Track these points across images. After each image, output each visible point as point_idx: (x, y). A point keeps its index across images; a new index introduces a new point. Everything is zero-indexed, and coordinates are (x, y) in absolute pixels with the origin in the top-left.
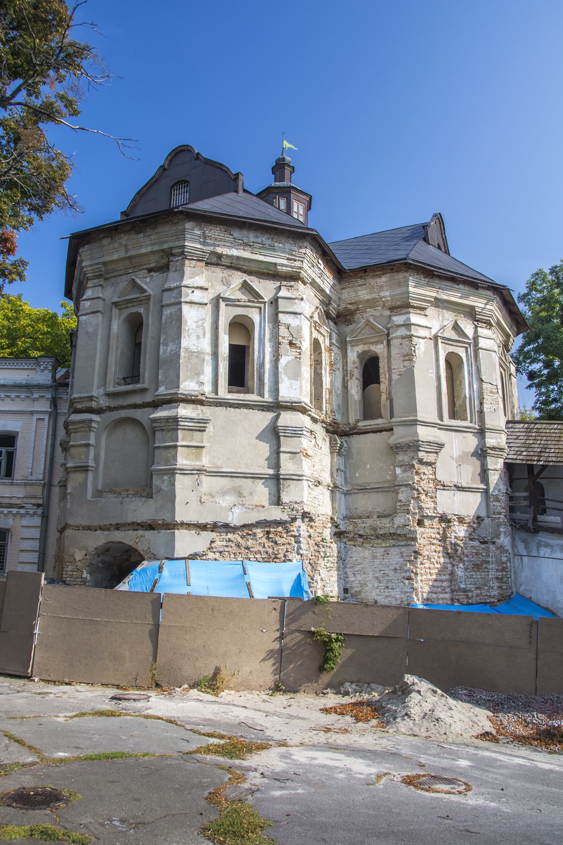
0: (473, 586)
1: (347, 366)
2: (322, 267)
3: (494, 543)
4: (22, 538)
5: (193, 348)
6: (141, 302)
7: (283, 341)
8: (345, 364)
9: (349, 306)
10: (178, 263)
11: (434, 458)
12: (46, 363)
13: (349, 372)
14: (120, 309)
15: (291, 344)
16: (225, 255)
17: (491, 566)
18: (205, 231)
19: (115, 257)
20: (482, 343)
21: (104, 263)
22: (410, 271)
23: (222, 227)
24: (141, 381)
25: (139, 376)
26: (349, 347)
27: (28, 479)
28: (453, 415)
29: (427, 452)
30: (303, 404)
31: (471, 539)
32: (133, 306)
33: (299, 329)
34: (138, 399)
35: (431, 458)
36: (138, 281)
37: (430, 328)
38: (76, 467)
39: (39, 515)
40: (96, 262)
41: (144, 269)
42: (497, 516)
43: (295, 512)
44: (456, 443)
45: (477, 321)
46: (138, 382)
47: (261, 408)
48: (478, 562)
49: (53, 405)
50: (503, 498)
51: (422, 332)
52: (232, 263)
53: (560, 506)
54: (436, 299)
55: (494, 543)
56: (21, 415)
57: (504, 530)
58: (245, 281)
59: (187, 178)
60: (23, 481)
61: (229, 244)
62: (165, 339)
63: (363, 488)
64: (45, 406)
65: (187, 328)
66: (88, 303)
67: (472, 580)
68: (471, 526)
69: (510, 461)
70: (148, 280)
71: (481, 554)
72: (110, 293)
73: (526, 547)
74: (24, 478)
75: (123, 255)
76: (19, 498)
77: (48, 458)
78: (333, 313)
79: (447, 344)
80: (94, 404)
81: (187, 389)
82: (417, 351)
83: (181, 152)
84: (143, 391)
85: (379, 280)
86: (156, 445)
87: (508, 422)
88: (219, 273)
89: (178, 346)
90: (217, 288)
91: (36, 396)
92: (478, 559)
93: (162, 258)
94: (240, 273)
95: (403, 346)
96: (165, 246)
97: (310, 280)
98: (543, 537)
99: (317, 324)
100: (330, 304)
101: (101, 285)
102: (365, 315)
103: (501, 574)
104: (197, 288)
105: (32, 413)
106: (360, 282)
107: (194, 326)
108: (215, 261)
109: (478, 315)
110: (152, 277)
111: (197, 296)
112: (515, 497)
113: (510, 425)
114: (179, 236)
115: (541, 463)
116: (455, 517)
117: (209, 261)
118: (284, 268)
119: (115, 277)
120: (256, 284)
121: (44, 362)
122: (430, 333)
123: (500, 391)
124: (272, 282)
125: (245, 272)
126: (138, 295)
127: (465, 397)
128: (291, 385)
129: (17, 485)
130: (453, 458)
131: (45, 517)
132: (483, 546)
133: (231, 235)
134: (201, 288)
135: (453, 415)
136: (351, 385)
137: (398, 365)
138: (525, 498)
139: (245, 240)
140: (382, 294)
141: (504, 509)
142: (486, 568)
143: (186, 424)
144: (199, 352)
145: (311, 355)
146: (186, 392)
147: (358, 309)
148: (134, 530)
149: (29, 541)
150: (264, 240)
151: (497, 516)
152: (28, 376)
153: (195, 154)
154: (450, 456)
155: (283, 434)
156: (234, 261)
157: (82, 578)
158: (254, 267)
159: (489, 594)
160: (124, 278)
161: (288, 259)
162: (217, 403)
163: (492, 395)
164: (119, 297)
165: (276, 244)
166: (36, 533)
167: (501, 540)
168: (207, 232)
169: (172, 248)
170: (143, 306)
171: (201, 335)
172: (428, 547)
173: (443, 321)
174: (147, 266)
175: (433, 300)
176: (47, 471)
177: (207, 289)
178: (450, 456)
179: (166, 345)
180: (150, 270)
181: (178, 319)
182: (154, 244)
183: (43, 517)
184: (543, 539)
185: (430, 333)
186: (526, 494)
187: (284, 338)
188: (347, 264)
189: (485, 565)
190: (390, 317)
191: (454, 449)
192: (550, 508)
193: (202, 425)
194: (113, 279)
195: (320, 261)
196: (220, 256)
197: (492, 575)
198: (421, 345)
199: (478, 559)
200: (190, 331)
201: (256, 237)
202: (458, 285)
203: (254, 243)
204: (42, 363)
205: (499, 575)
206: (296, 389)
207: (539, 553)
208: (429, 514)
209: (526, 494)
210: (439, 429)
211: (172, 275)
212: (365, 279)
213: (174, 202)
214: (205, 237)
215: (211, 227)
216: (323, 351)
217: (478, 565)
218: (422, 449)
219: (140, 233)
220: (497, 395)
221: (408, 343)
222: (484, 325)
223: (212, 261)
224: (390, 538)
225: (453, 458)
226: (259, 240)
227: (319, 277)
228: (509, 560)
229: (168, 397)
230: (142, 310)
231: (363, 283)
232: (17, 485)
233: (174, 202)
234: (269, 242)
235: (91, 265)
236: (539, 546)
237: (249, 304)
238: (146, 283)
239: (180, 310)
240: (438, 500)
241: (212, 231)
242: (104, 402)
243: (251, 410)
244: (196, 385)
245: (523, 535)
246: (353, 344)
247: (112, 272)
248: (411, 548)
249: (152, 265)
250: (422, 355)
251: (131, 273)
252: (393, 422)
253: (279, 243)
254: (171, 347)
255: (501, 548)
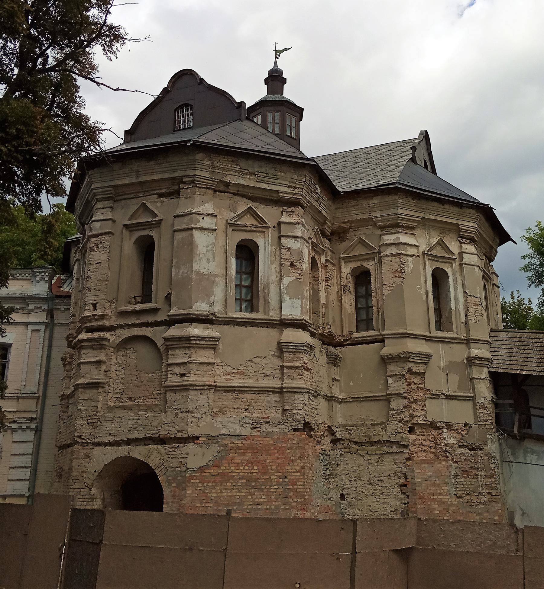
0: (463, 492)
1: (341, 281)
2: (319, 192)
3: (481, 449)
4: (12, 455)
5: (204, 271)
6: (153, 226)
7: (285, 263)
8: (339, 279)
9: (343, 225)
10: (189, 191)
11: (423, 368)
12: (43, 274)
13: (342, 287)
14: (131, 231)
15: (292, 265)
16: (232, 183)
17: (480, 473)
18: (214, 162)
19: (126, 181)
20: (467, 258)
21: (115, 187)
22: (399, 194)
23: (229, 157)
24: (153, 300)
25: (152, 295)
26: (343, 263)
27: (22, 392)
28: (439, 328)
29: (416, 363)
30: (303, 321)
31: (460, 446)
32: (144, 229)
33: (300, 253)
34: (151, 319)
35: (420, 369)
36: (148, 205)
37: (418, 246)
38: (87, 384)
39: (32, 430)
40: (106, 184)
41: (155, 194)
42: (484, 423)
43: (297, 423)
44: (442, 354)
45: (461, 237)
46: (150, 301)
47: (265, 325)
48: (468, 469)
49: (49, 316)
50: (490, 406)
51: (411, 251)
52: (238, 191)
53: (542, 413)
54: (423, 218)
55: (481, 449)
56: (15, 326)
57: (491, 436)
58: (250, 207)
59: (191, 103)
60: (16, 395)
61: (236, 174)
62: (177, 263)
63: (357, 396)
64: (42, 317)
65: (198, 252)
66: (98, 224)
67: (462, 486)
68: (459, 433)
69: (495, 370)
70: (159, 204)
71: (469, 460)
72: (123, 215)
73: (513, 454)
74: (16, 391)
75: (134, 180)
76: (11, 412)
77: (43, 370)
78: (328, 232)
79: (433, 260)
80: (107, 323)
81: (198, 309)
82: (406, 268)
83: (185, 78)
84: (155, 311)
85: (371, 202)
86: (170, 362)
87: (492, 330)
88: (226, 200)
89: (190, 269)
90: (225, 214)
91: (31, 307)
92: (468, 466)
93: (173, 185)
94: (245, 200)
95: (393, 263)
96: (176, 174)
97: (309, 205)
98: (528, 444)
99: (314, 244)
100: (325, 223)
101: (111, 207)
102: (358, 233)
103: (489, 480)
104: (208, 215)
105: (27, 324)
106: (354, 202)
107: (204, 250)
108: (222, 188)
109: (462, 231)
110: (162, 202)
111: (207, 222)
112: (500, 404)
113: (493, 334)
114: (189, 166)
115: (524, 373)
116: (444, 425)
117: (217, 189)
118: (286, 195)
119: (125, 199)
120: (262, 210)
121: (40, 273)
122: (418, 251)
123: (484, 304)
124: (274, 208)
125: (249, 198)
126: (150, 220)
127: (451, 309)
128: (292, 303)
129: (7, 399)
130: (440, 368)
131: (38, 431)
132: (472, 452)
133: (237, 165)
134: (210, 215)
135: (439, 328)
136: (345, 299)
137: (388, 279)
138: (511, 405)
139: (251, 170)
140: (374, 215)
141: (490, 416)
142: (475, 474)
143: (198, 342)
144: (209, 275)
145: (310, 273)
146: (198, 313)
147: (351, 228)
148: (145, 445)
149: (20, 457)
150: (267, 169)
151: (484, 423)
152: (23, 286)
153: (198, 79)
154: (438, 366)
155: (285, 350)
156: (240, 189)
157: (90, 495)
158: (259, 194)
159: (479, 501)
160: (134, 201)
161: (289, 187)
162: (226, 321)
163: (477, 307)
164: (130, 220)
165: (278, 173)
166: (29, 448)
167: (489, 446)
168: (216, 162)
169: (182, 176)
170: (155, 229)
171: (211, 258)
172: (419, 454)
173: (429, 239)
174: (158, 191)
175: (420, 220)
176: (42, 383)
177: (216, 216)
178: (438, 366)
179: (179, 268)
180: (160, 196)
181: (191, 244)
182: (164, 172)
183: (36, 432)
184: (528, 446)
185: (418, 251)
186: (511, 401)
187: (285, 260)
188: (342, 186)
189: (474, 472)
190: (381, 236)
191: (442, 359)
192: (534, 416)
193: (213, 343)
194: (123, 201)
195: (317, 187)
196: (227, 184)
197: (481, 481)
198: (409, 263)
199: (468, 466)
200: (201, 256)
201: (261, 167)
202: (443, 205)
203: (258, 172)
204: (38, 274)
205: (488, 481)
206: (297, 307)
207: (525, 459)
208: (420, 422)
209: (511, 401)
210: (427, 340)
211: (182, 201)
212: (358, 201)
213: (178, 124)
214: (214, 167)
215: (219, 158)
216: (320, 268)
217: (467, 471)
218: (412, 360)
219: (151, 160)
220: (481, 308)
221: (397, 260)
222: (468, 241)
223: (220, 189)
224: (384, 445)
225: (440, 368)
226: (263, 170)
227: (316, 201)
228: (497, 466)
229: (181, 317)
230: (153, 233)
231: (356, 204)
232: (9, 398)
233: (178, 124)
234: (272, 172)
235: (101, 188)
236: (525, 452)
237: (254, 229)
238: (157, 208)
239: (192, 235)
240: (427, 408)
241: (221, 161)
242: (113, 321)
243: (256, 328)
244: (207, 306)
245: (512, 442)
246: (346, 260)
247: (122, 195)
248: (403, 455)
249: (163, 191)
250: (410, 272)
251: (142, 197)
252: (384, 335)
253: (282, 172)
254: (183, 270)
255: (489, 454)
